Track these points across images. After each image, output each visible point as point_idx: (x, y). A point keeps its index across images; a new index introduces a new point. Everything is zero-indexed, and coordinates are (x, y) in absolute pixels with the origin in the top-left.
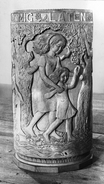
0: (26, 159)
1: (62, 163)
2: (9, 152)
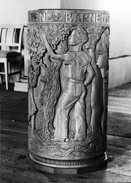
0: (49, 162)
1: (65, 165)
2: (7, 149)
